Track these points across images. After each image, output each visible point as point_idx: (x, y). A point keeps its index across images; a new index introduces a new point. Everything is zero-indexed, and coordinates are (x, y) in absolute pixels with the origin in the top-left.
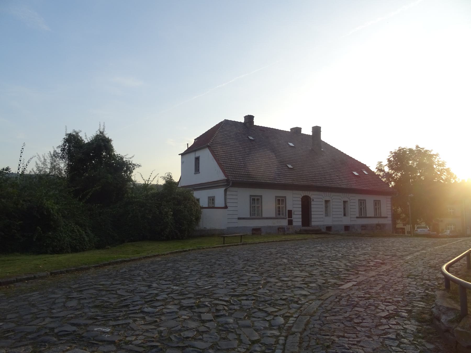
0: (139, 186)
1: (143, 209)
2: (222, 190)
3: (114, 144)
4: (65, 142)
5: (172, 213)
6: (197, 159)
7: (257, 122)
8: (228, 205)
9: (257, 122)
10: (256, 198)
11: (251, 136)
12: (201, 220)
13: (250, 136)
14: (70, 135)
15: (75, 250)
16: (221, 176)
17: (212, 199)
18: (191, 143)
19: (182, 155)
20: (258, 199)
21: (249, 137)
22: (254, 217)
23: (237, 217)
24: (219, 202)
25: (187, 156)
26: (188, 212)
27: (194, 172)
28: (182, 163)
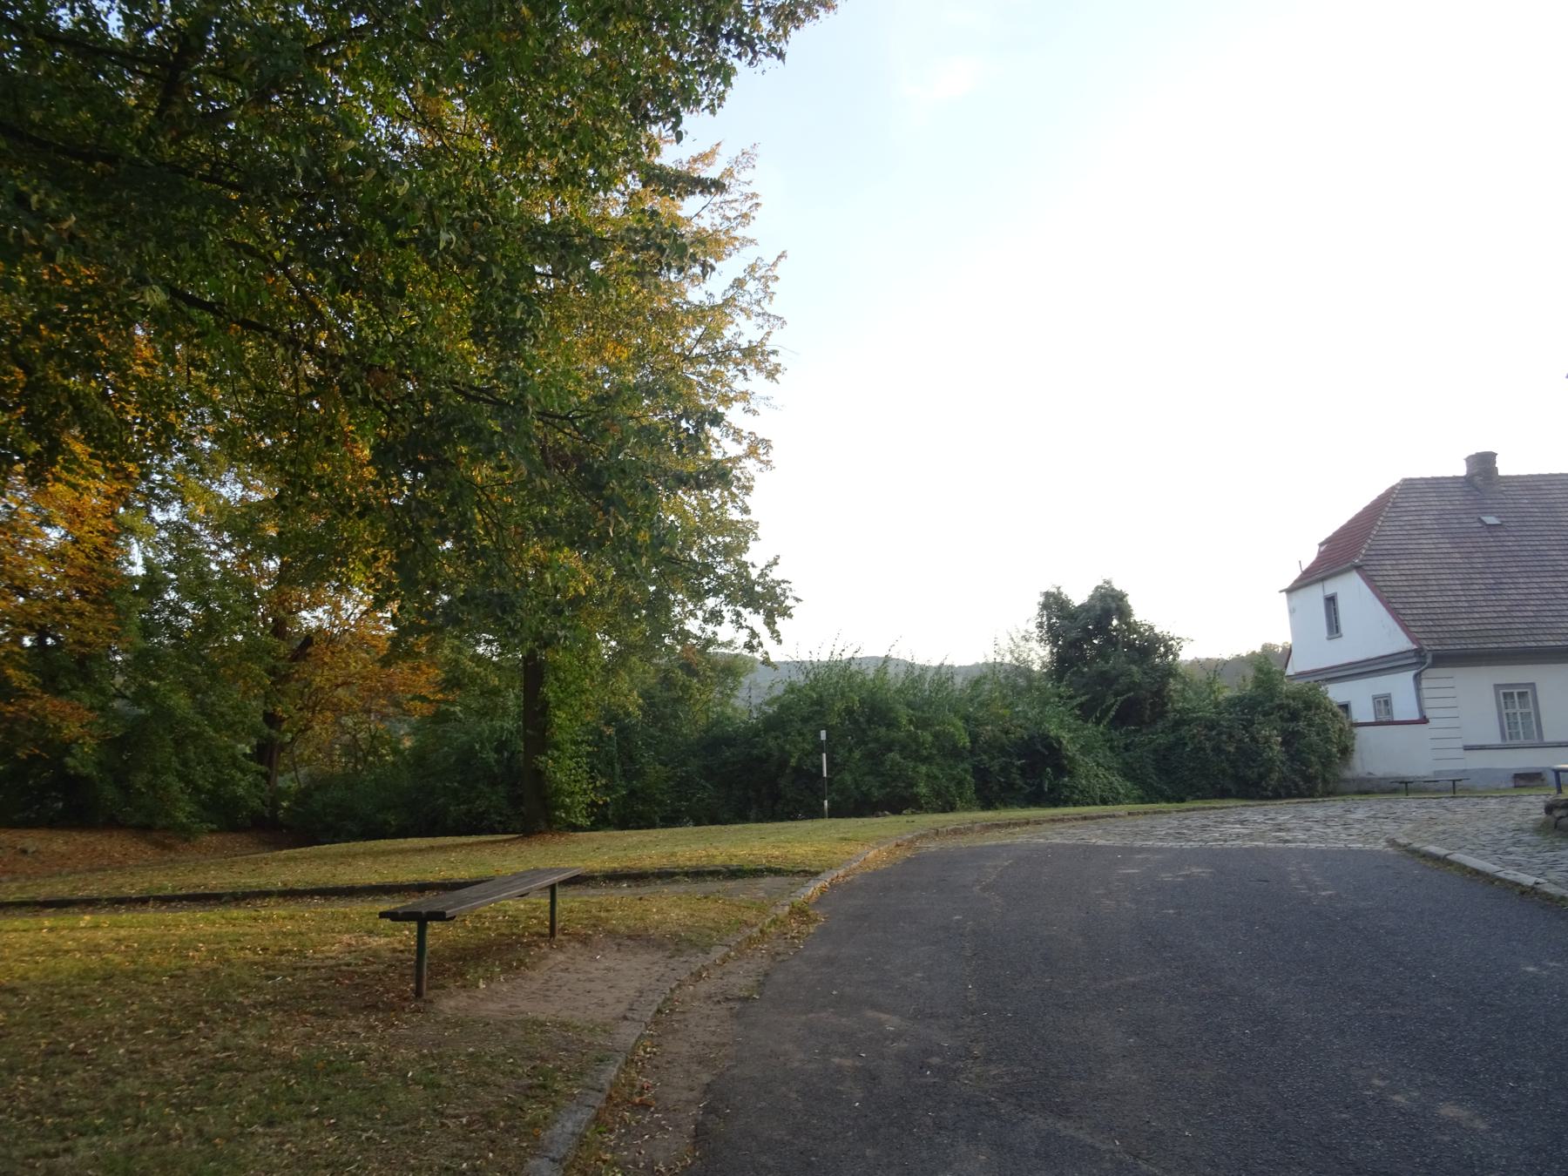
0: (977, 683)
1: (1214, 733)
2: (1407, 677)
3: (1131, 601)
4: (1042, 610)
5: (1280, 739)
6: (1331, 601)
7: (1505, 468)
8: (1429, 714)
9: (1505, 468)
10: (1516, 691)
11: (1491, 514)
12: (1356, 756)
13: (1485, 514)
14: (1047, 595)
15: (1104, 802)
16: (1400, 642)
17: (1383, 702)
18: (1309, 556)
19: (1290, 591)
20: (1521, 695)
21: (1484, 518)
22: (1515, 742)
23: (1460, 744)
24: (1405, 707)
25: (1301, 593)
26: (1318, 735)
27: (1326, 635)
28: (1292, 611)
